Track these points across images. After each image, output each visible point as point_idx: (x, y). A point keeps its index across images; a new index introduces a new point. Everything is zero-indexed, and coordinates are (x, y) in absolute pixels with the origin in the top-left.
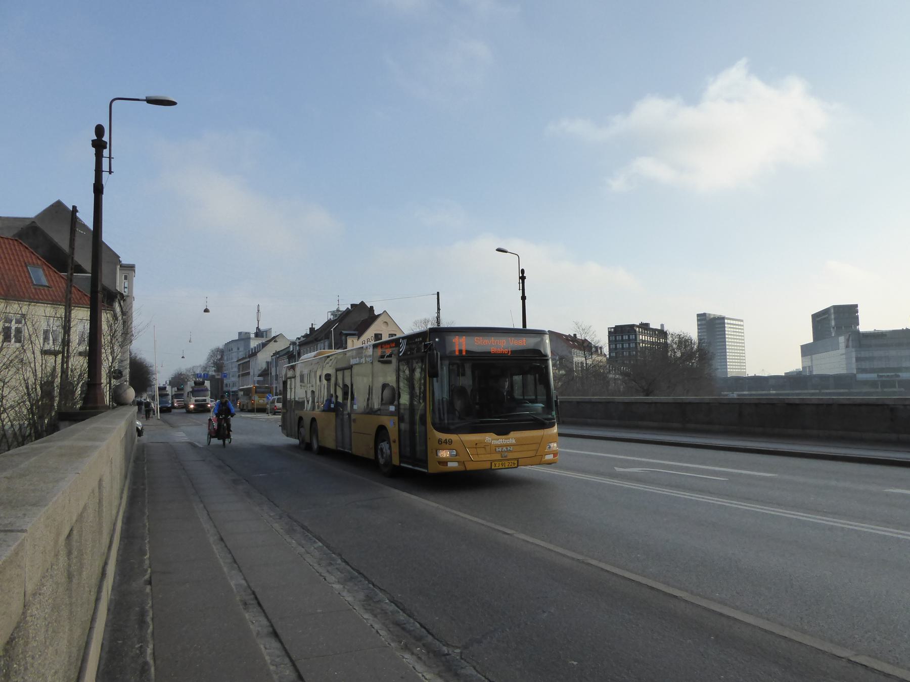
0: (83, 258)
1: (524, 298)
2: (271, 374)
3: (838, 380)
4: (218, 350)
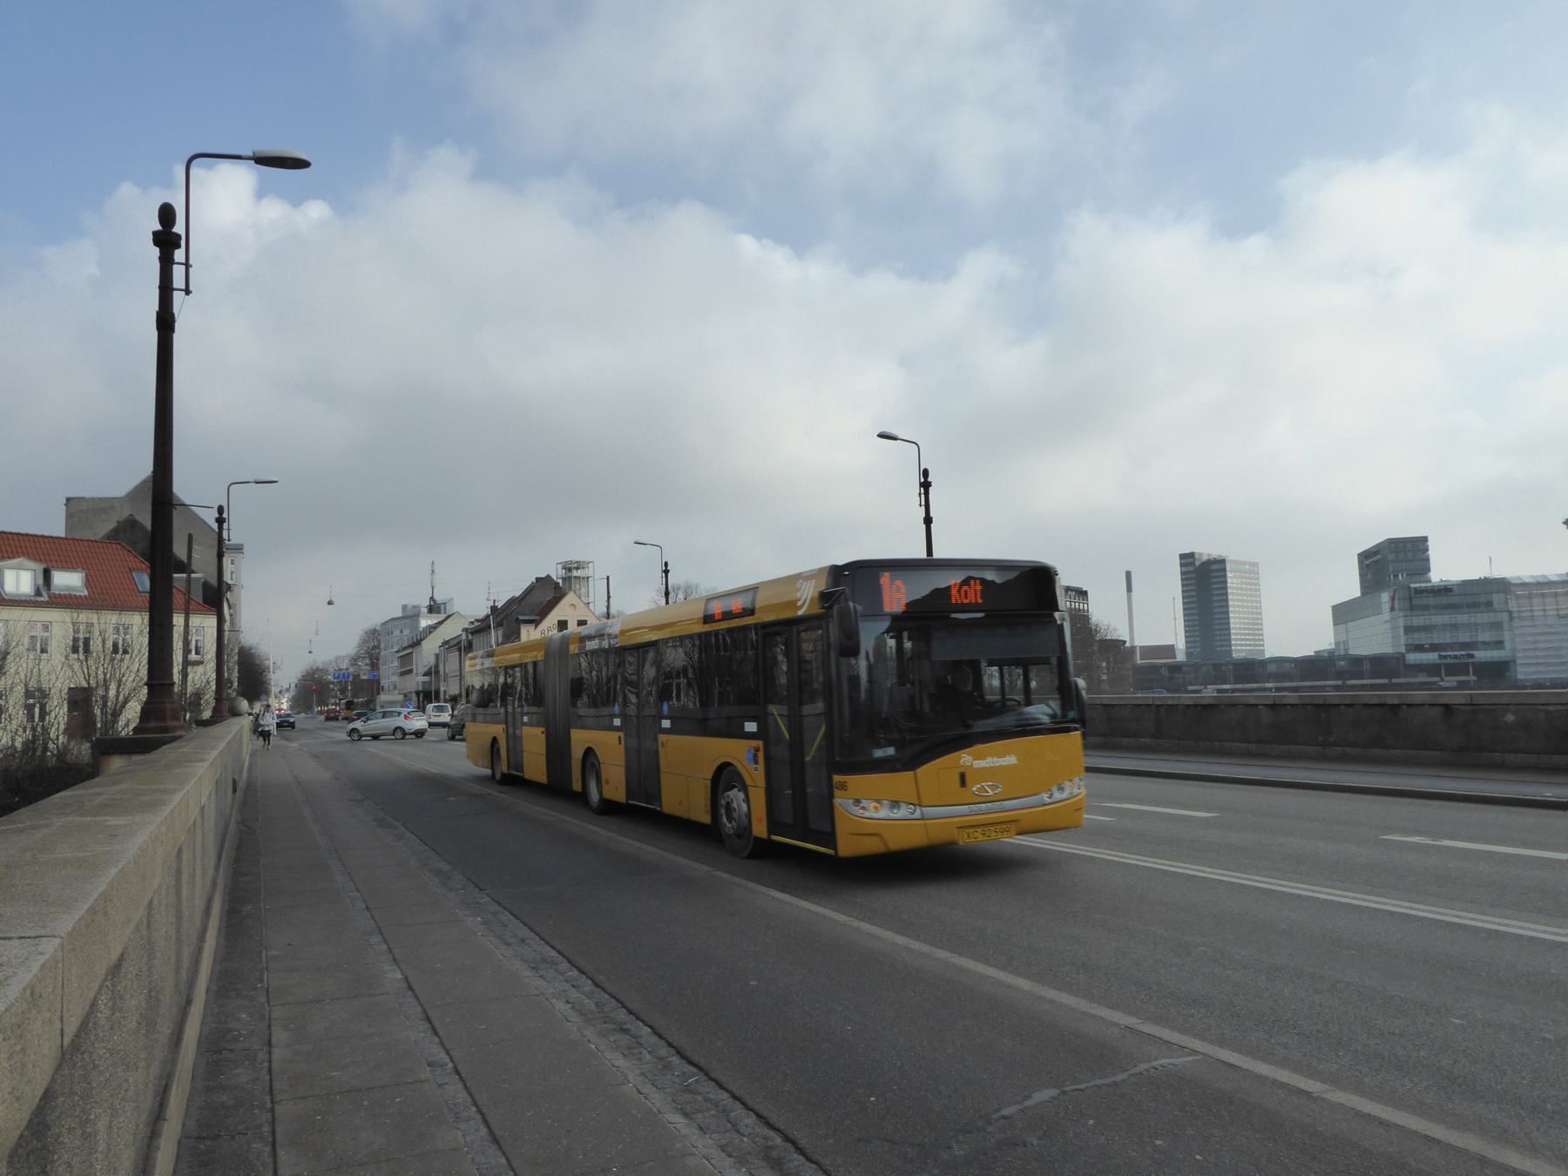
1: (928, 521)
3: (1381, 665)
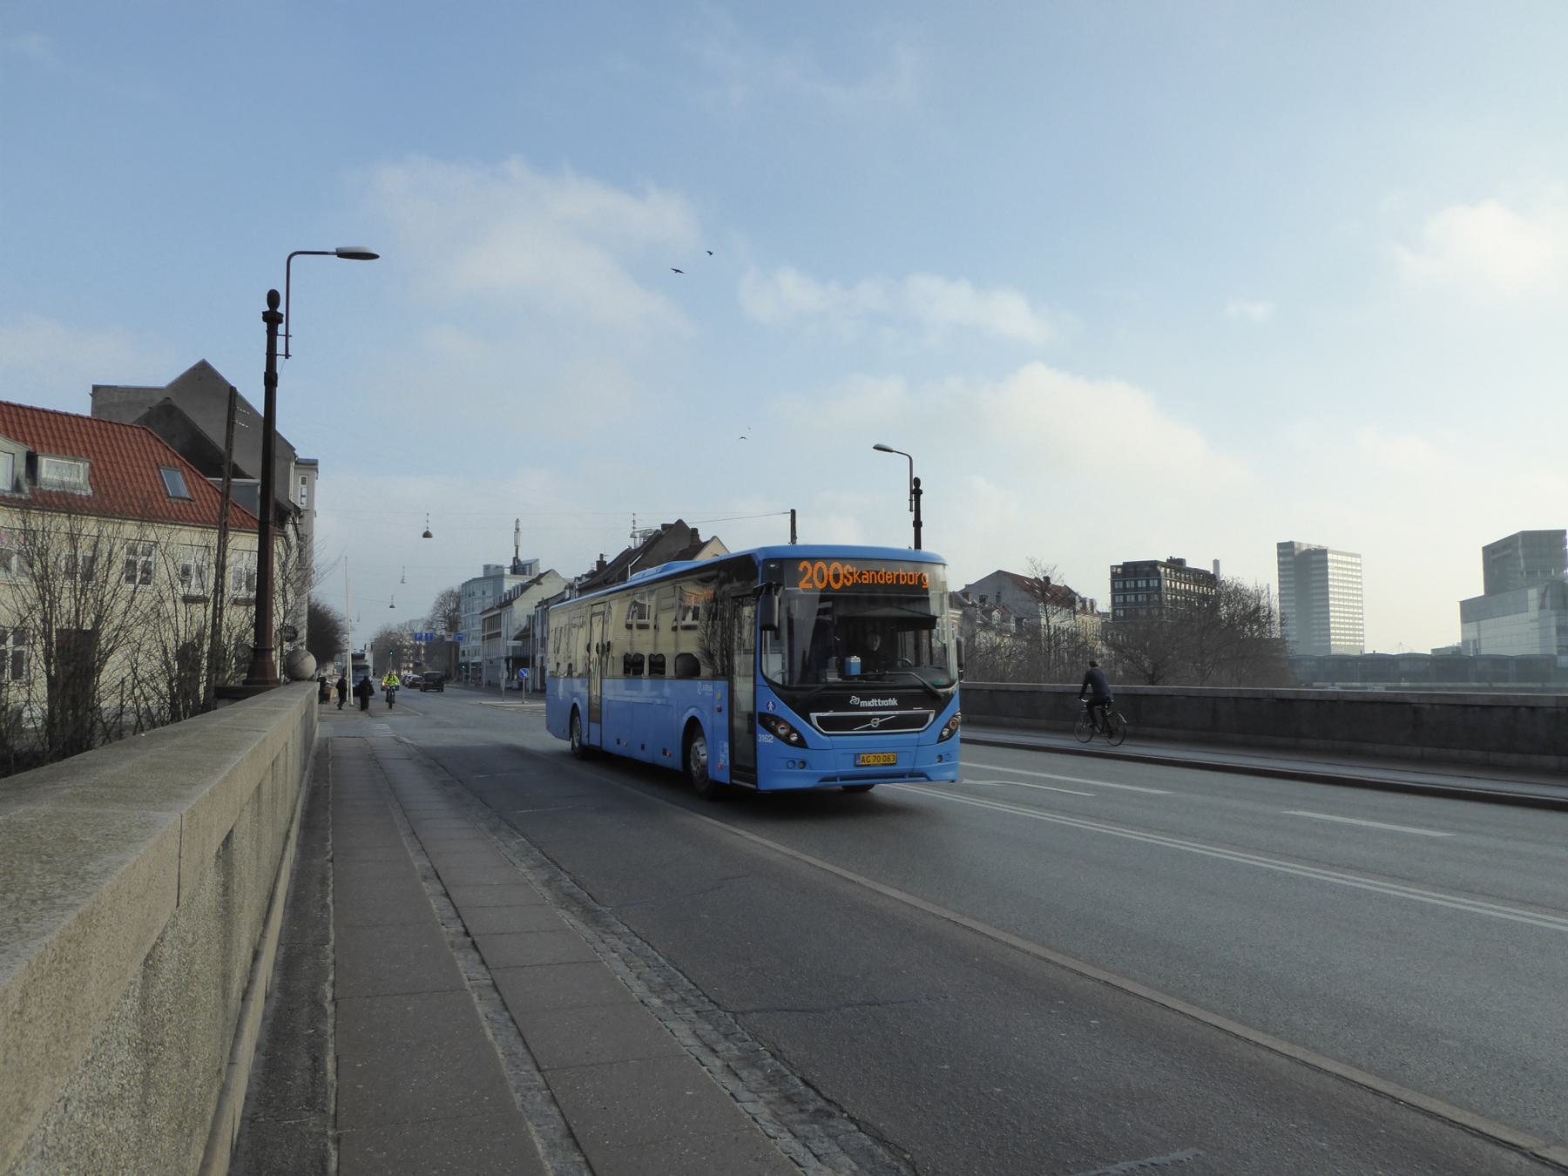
0: (248, 459)
1: (918, 524)
2: (534, 635)
3: (1525, 666)
4: (451, 594)
